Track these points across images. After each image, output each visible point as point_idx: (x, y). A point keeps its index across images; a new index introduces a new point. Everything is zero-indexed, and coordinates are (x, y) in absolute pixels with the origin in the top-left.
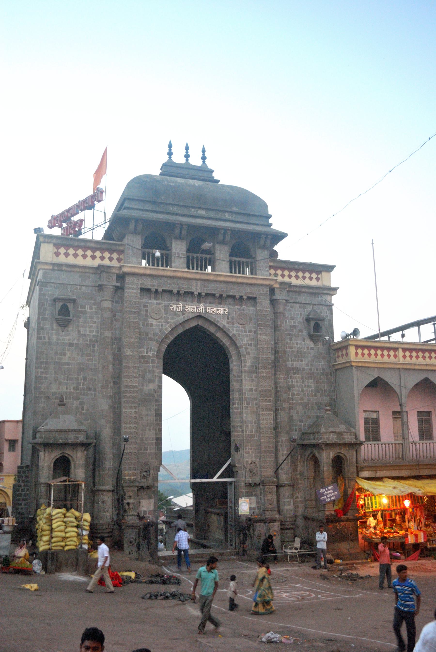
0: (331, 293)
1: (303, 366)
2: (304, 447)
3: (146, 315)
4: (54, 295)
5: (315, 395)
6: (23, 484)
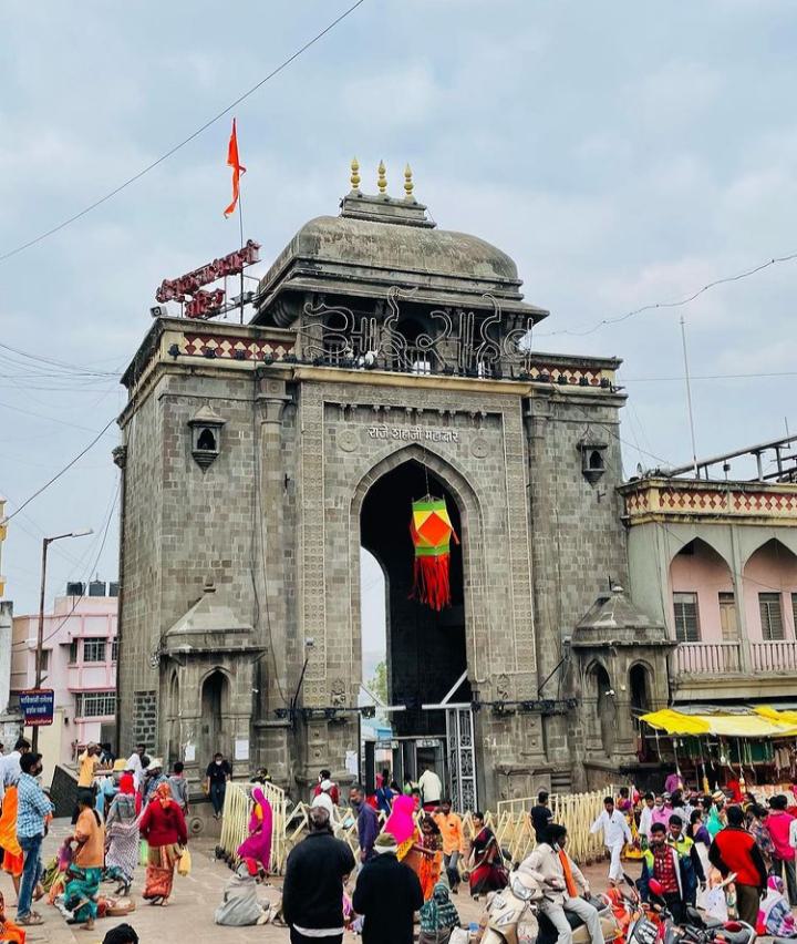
0: (617, 403)
1: (574, 522)
2: (581, 651)
3: (333, 445)
4: (188, 415)
5: (596, 568)
6: (146, 720)
